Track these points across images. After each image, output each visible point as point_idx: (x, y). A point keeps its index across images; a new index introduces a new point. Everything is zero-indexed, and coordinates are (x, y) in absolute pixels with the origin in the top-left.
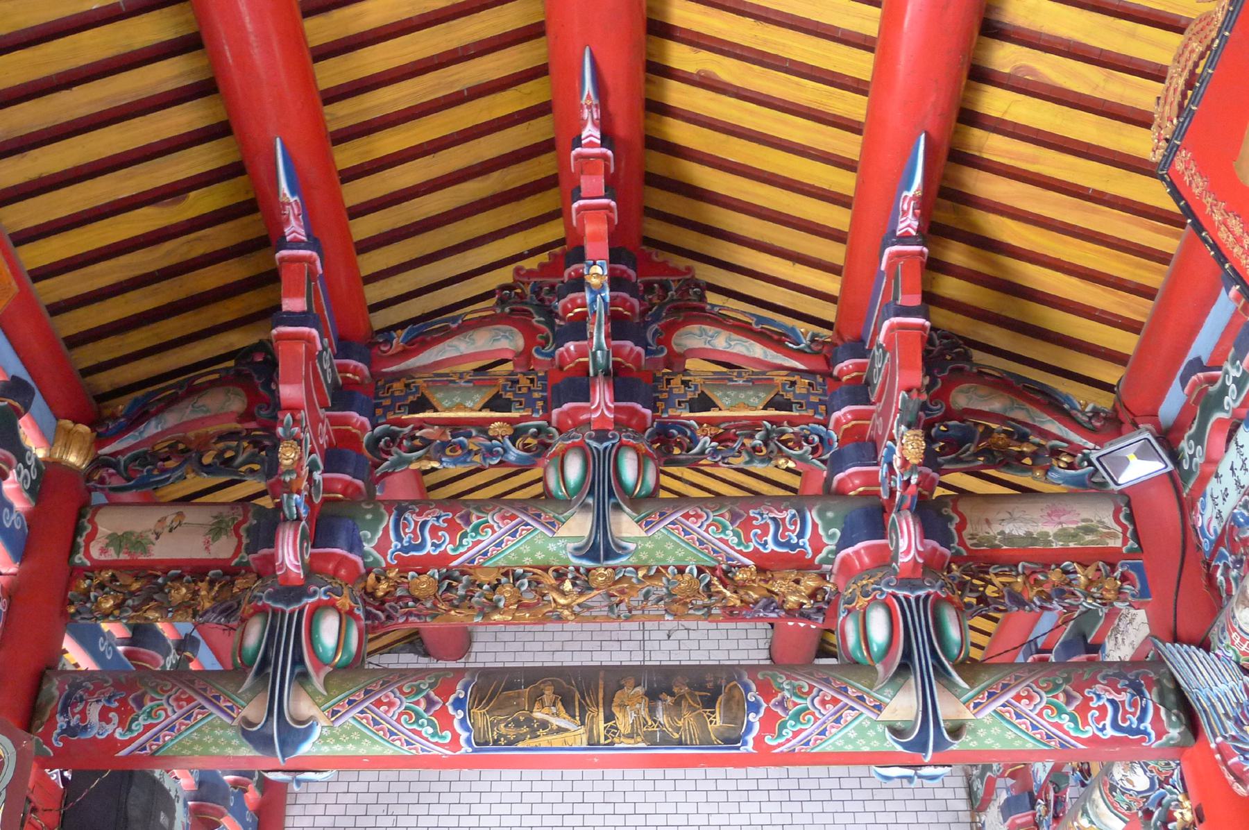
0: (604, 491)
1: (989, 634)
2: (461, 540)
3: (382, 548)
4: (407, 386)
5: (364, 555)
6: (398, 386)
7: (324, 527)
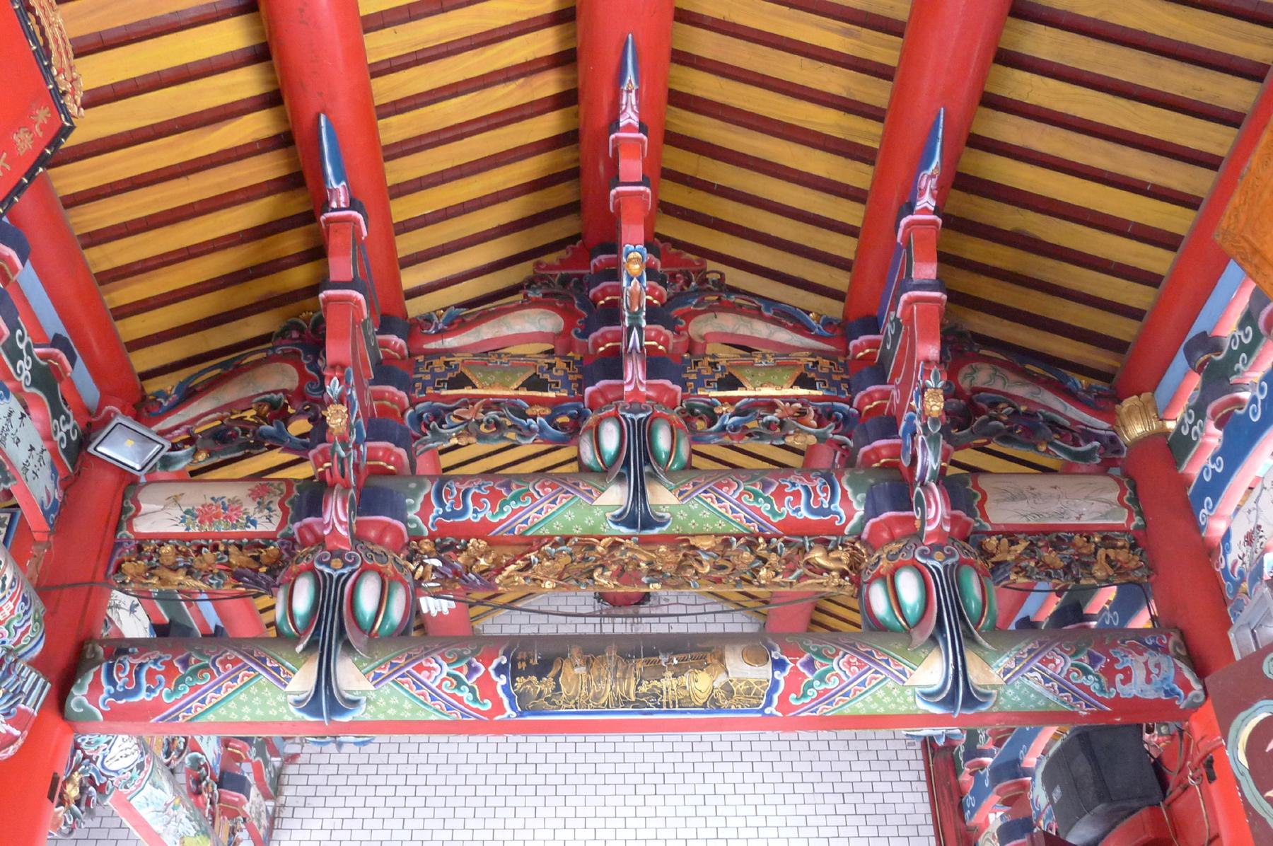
0: (637, 462)
1: (262, 611)
2: (501, 508)
3: (424, 514)
4: (447, 363)
5: (405, 521)
6: (438, 365)
7: (373, 496)
